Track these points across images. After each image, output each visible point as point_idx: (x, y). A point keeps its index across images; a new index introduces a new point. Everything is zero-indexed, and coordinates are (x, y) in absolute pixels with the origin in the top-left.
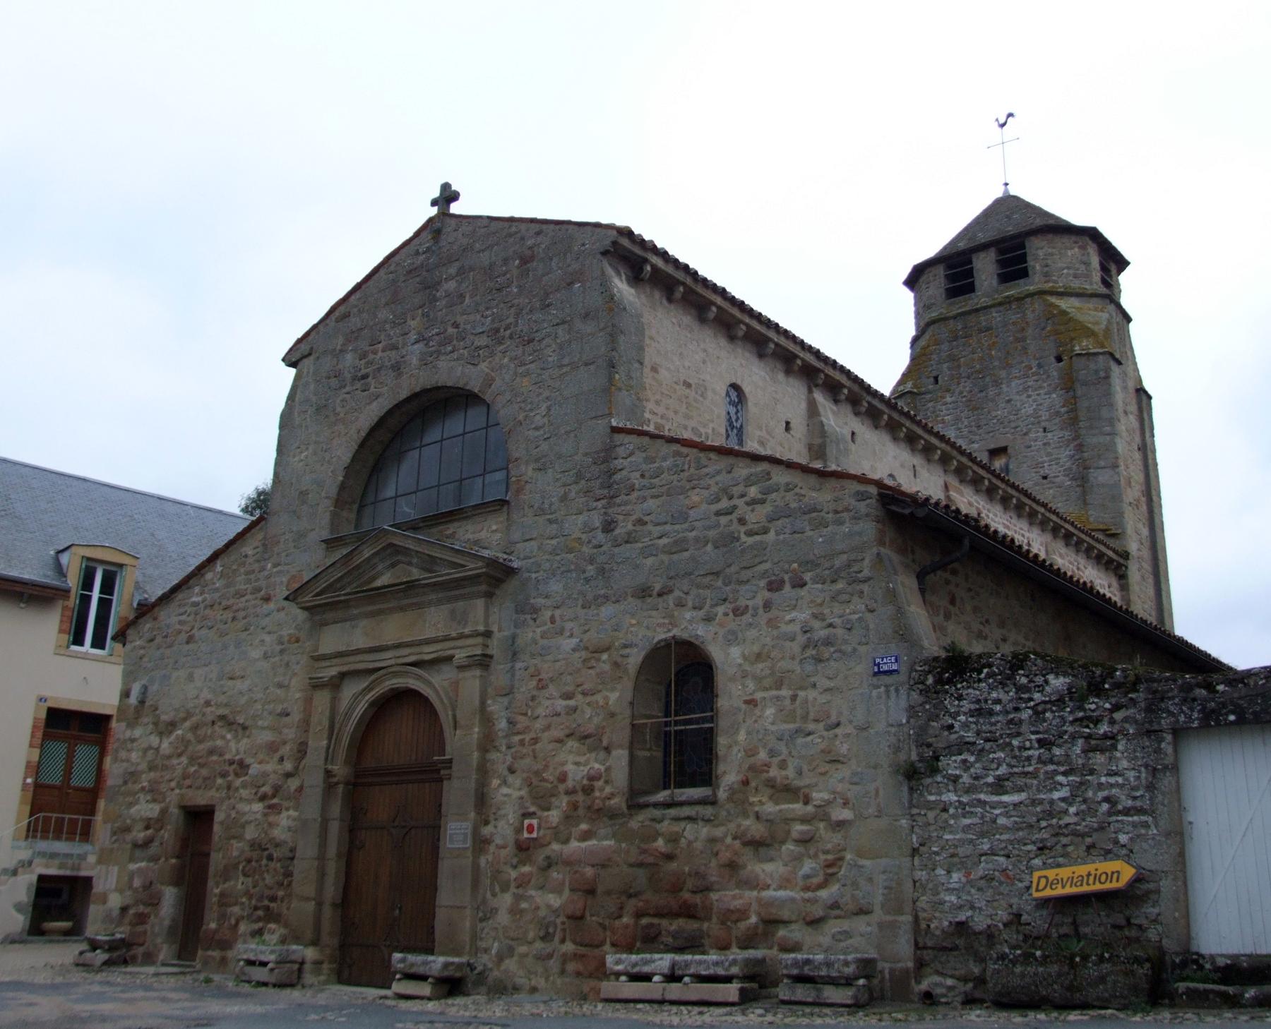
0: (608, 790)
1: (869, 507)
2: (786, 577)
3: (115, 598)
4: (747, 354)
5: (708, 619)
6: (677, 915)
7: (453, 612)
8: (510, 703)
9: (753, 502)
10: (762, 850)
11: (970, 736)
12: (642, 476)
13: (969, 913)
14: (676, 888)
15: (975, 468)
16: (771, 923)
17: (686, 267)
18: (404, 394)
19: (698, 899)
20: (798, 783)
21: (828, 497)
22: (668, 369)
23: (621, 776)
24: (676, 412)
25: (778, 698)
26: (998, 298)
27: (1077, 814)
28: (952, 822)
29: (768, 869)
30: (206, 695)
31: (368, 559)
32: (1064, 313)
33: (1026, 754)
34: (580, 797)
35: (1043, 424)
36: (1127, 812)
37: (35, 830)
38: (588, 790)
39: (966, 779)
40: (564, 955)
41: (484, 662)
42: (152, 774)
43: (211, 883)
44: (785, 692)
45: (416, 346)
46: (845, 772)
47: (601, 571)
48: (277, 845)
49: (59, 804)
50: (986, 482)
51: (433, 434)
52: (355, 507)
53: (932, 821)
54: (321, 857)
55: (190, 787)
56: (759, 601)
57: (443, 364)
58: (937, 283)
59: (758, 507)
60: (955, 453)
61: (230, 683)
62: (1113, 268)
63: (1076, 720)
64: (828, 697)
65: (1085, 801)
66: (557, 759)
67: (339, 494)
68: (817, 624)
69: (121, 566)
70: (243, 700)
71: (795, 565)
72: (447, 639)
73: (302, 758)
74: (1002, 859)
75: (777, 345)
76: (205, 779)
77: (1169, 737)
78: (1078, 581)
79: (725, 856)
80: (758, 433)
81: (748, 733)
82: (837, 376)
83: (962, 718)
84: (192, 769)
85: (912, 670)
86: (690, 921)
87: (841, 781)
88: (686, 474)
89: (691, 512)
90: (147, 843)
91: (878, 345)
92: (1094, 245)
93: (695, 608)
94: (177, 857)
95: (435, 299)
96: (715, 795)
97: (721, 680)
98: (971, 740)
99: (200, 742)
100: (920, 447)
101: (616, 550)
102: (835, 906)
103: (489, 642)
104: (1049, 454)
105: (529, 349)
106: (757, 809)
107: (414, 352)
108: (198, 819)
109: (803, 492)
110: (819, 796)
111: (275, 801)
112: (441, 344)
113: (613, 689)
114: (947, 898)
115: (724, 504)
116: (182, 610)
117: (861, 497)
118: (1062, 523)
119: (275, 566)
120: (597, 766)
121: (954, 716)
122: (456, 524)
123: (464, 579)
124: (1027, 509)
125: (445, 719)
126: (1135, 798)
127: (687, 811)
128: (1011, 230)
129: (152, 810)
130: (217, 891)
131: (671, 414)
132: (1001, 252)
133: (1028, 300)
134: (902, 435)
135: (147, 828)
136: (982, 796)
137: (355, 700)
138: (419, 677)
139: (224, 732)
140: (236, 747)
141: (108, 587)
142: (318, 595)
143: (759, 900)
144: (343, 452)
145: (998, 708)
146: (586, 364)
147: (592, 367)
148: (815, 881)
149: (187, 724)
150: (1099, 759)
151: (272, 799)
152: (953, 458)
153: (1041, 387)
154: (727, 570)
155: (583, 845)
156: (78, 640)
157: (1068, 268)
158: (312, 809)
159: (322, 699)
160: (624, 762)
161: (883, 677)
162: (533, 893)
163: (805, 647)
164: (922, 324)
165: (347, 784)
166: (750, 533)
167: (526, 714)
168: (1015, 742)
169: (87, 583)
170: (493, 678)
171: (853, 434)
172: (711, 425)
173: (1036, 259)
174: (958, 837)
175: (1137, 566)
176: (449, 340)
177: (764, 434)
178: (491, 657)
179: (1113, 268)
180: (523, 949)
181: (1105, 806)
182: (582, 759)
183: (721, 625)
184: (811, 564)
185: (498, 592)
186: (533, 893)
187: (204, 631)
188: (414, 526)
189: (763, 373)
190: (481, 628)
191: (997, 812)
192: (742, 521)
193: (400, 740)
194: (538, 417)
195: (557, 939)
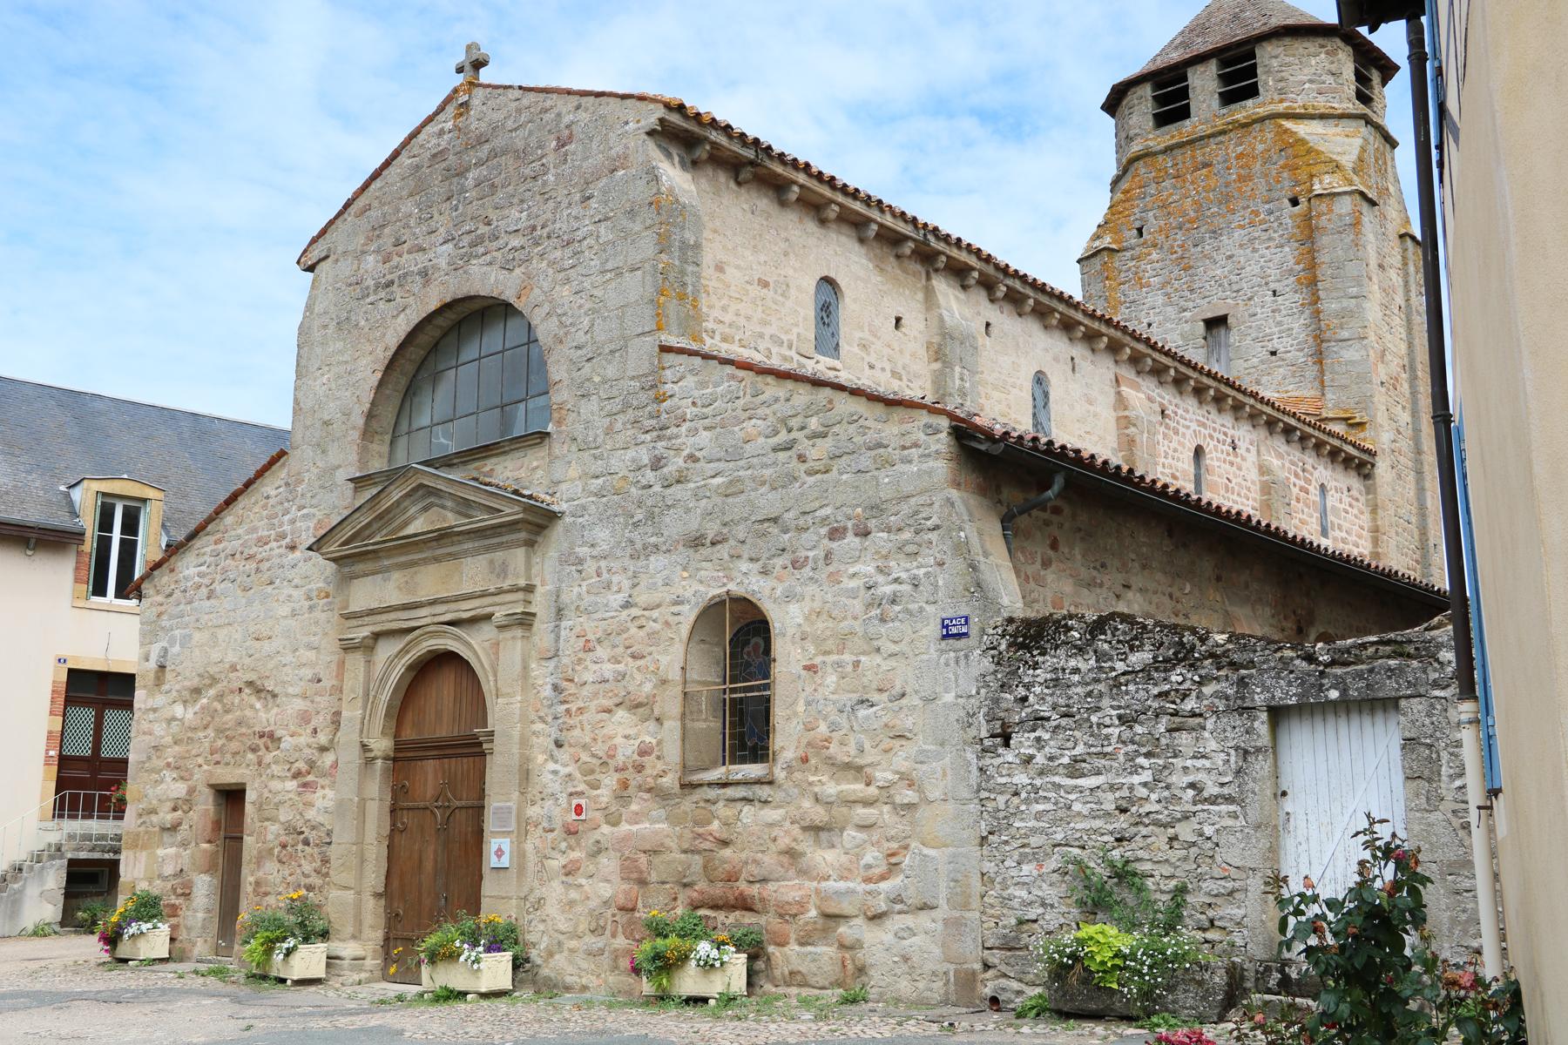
0: (660, 766)
1: (942, 442)
2: (850, 524)
3: (140, 539)
4: (843, 239)
5: (765, 572)
6: (733, 908)
7: (491, 562)
8: (556, 667)
9: (815, 436)
10: (824, 835)
11: (1044, 709)
12: (694, 404)
13: (1041, 910)
14: (732, 878)
15: (1156, 356)
16: (832, 918)
17: (756, 141)
18: (433, 305)
19: (755, 890)
20: (860, 761)
21: (896, 430)
22: (738, 267)
23: (673, 752)
24: (748, 318)
25: (839, 664)
26: (1220, 124)
27: (1159, 801)
28: (1023, 808)
29: (824, 857)
30: (231, 658)
31: (398, 503)
32: (1303, 142)
33: (1105, 731)
34: (630, 774)
35: (1273, 286)
36: (1213, 800)
37: (62, 808)
38: (640, 768)
39: (1040, 759)
40: (616, 950)
41: (525, 621)
42: (177, 748)
43: (245, 870)
44: (848, 657)
45: (445, 247)
46: (911, 749)
47: (651, 516)
48: (313, 828)
49: (88, 781)
50: (1172, 372)
51: (470, 351)
52: (388, 438)
53: (1002, 806)
54: (359, 842)
55: (218, 763)
56: (819, 553)
57: (475, 267)
58: (1143, 104)
59: (819, 441)
60: (1127, 339)
61: (257, 644)
62: (1376, 77)
63: (1160, 695)
64: (893, 663)
65: (1168, 787)
66: (605, 731)
67: (366, 424)
68: (881, 579)
69: (144, 500)
70: (271, 665)
71: (859, 510)
72: (484, 594)
73: (337, 730)
74: (1076, 851)
75: (881, 225)
76: (235, 754)
77: (1264, 716)
78: (1228, 512)
79: (784, 842)
80: (858, 334)
81: (808, 704)
82: (963, 256)
83: (1038, 689)
84: (220, 743)
85: (983, 632)
86: (748, 914)
87: (906, 759)
88: (741, 402)
89: (747, 446)
90: (174, 828)
91: (1043, 206)
92: (1349, 49)
93: (751, 560)
94: (209, 842)
95: (463, 190)
96: (771, 772)
97: (779, 647)
98: (1047, 714)
99: (227, 712)
100: (1080, 335)
101: (669, 491)
102: (898, 900)
103: (530, 597)
104: (1279, 324)
105: (568, 251)
106: (816, 789)
107: (443, 254)
108: (231, 797)
109: (867, 423)
110: (883, 776)
111: (310, 778)
112: (473, 245)
113: (665, 651)
114: (1017, 893)
115: (783, 437)
116: (201, 560)
117: (933, 431)
118: (1280, 416)
119: (301, 508)
120: (648, 739)
121: (1028, 687)
122: (494, 460)
123: (501, 525)
124: (1230, 401)
125: (488, 687)
126: (1222, 785)
127: (740, 792)
128: (1241, 34)
129: (179, 789)
130: (251, 879)
131: (742, 321)
132: (1224, 64)
133: (1257, 126)
134: (1054, 322)
135: (175, 809)
136: (1057, 779)
137: (392, 662)
138: (458, 638)
139: (253, 700)
140: (263, 715)
141: (130, 525)
142: (343, 544)
143: (817, 891)
144: (368, 371)
145: (1076, 678)
146: (632, 270)
147: (639, 273)
148: (877, 871)
149: (212, 692)
150: (1184, 739)
151: (305, 777)
152: (1124, 346)
153: (1270, 239)
154: (786, 516)
155: (635, 828)
156: (100, 590)
157: (1311, 81)
158: (348, 791)
159: (356, 661)
160: (677, 734)
161: (951, 641)
162: (583, 881)
163: (869, 606)
164: (1124, 161)
165: (386, 758)
166: (810, 473)
167: (571, 681)
168: (1094, 719)
169: (106, 523)
170: (536, 639)
171: (988, 325)
172: (795, 330)
173: (1268, 72)
174: (1030, 824)
175: (1388, 463)
176: (478, 241)
177: (866, 335)
178: (534, 615)
179: (1376, 77)
180: (573, 944)
181: (1191, 793)
182: (632, 732)
183: (779, 579)
184: (876, 509)
185: (540, 539)
186: (583, 881)
187: (227, 584)
188: (447, 462)
189: (864, 261)
190: (522, 582)
191: (1072, 797)
192: (802, 458)
193: (440, 713)
194: (581, 333)
195: (608, 932)
